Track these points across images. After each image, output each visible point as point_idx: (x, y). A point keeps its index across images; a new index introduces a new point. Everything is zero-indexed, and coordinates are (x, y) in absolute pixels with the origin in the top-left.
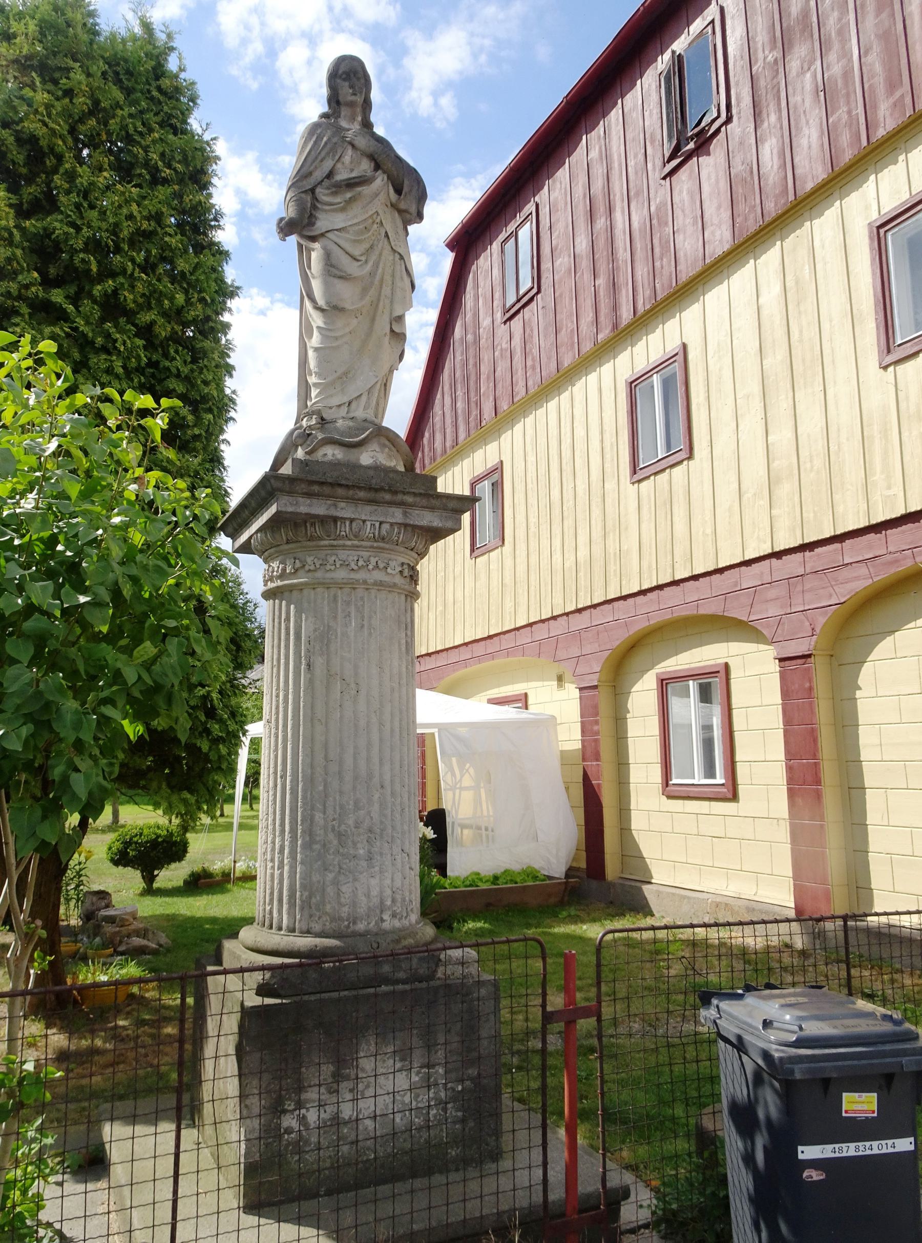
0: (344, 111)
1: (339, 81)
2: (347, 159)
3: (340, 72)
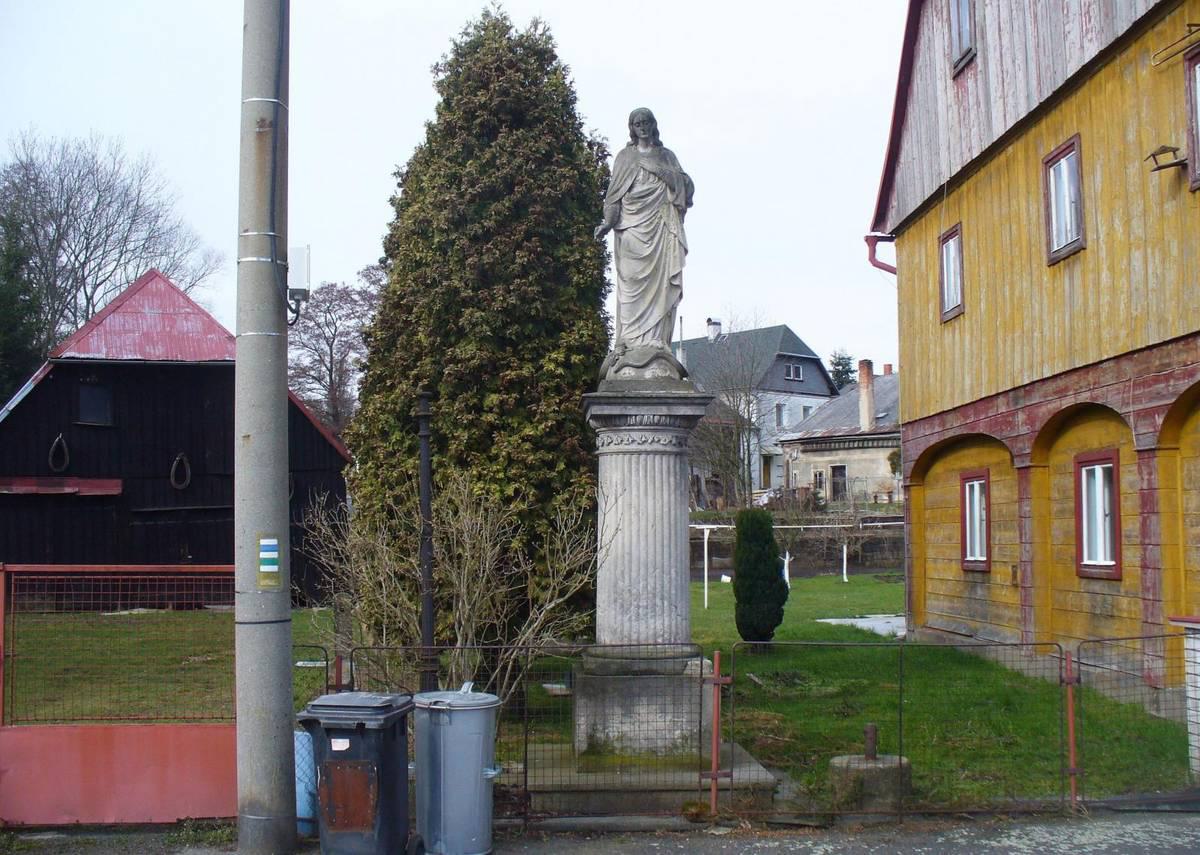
0: (640, 142)
2: (640, 177)
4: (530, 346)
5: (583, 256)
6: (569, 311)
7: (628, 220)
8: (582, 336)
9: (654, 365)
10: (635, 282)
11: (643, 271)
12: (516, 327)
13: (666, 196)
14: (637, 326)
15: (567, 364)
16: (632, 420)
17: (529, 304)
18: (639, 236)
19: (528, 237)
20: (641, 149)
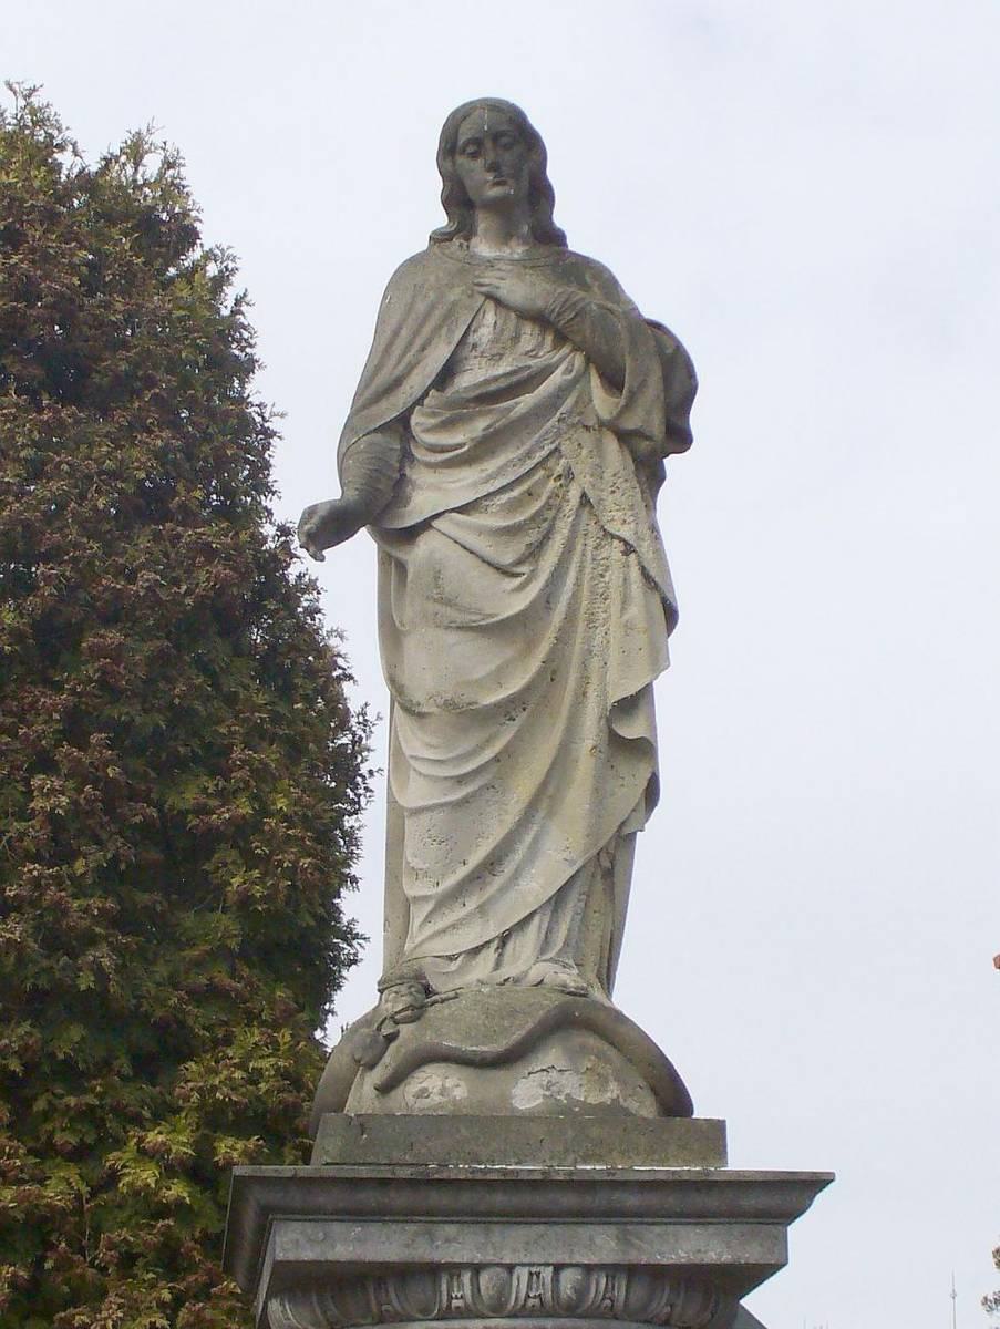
0: (483, 223)
1: (461, 160)
2: (485, 333)
3: (462, 140)
4: (72, 1101)
5: (264, 811)
6: (213, 993)
7: (436, 487)
8: (254, 1078)
9: (552, 1056)
10: (468, 717)
11: (498, 678)
12: (26, 1027)
13: (585, 401)
14: (472, 903)
15: (201, 1172)
16: (462, 1290)
17: (73, 955)
18: (483, 545)
19: (75, 728)
20: (483, 248)
